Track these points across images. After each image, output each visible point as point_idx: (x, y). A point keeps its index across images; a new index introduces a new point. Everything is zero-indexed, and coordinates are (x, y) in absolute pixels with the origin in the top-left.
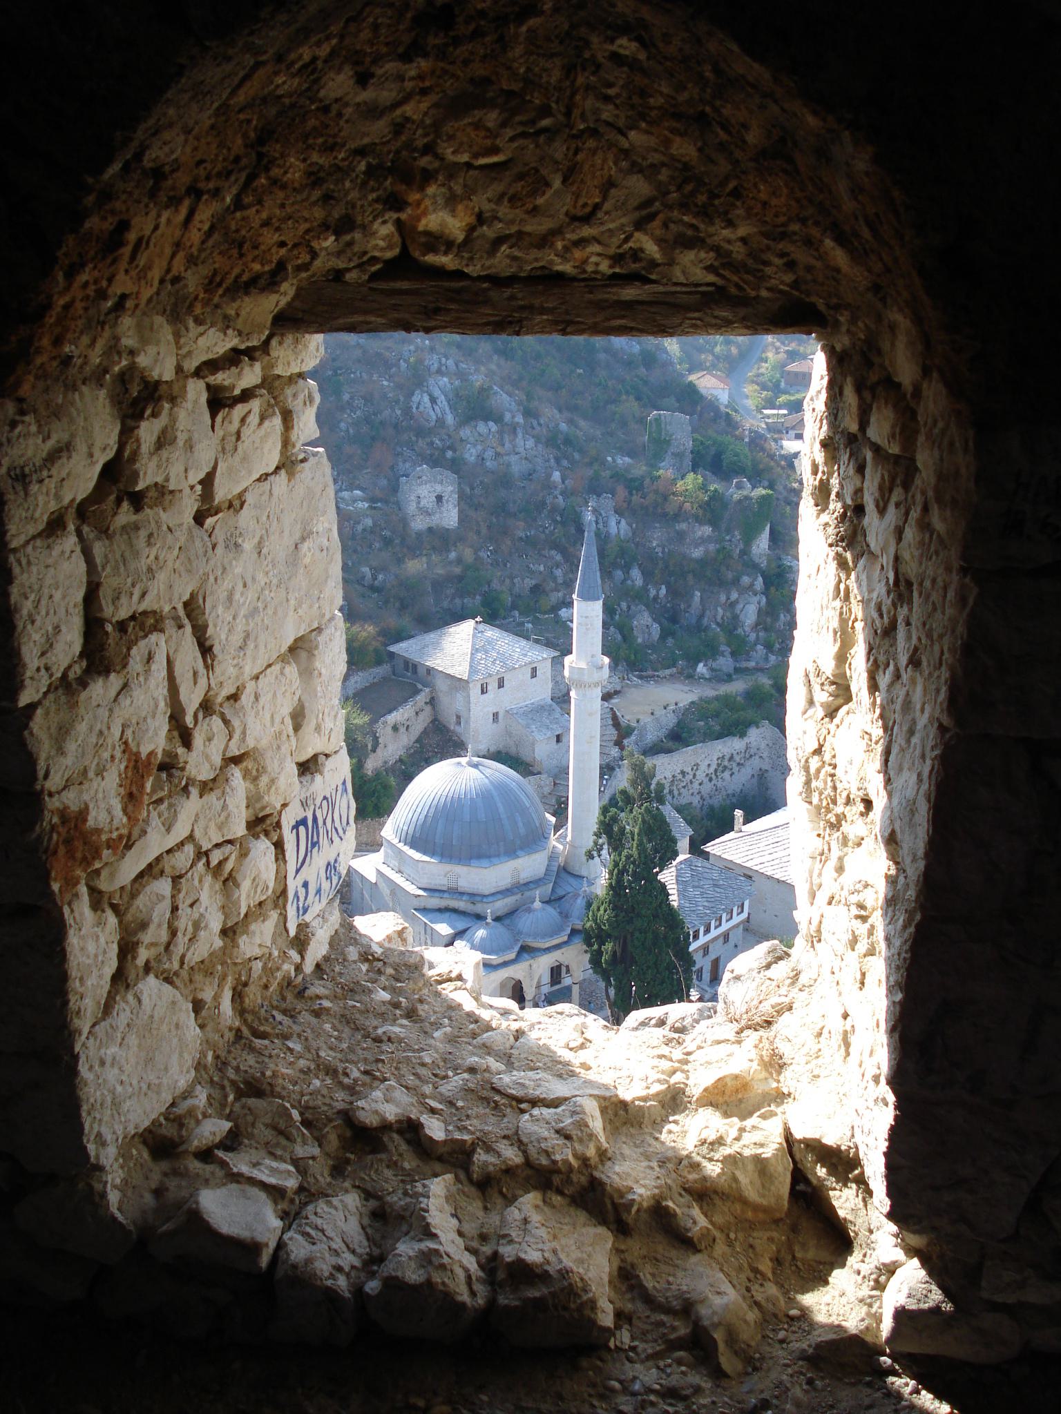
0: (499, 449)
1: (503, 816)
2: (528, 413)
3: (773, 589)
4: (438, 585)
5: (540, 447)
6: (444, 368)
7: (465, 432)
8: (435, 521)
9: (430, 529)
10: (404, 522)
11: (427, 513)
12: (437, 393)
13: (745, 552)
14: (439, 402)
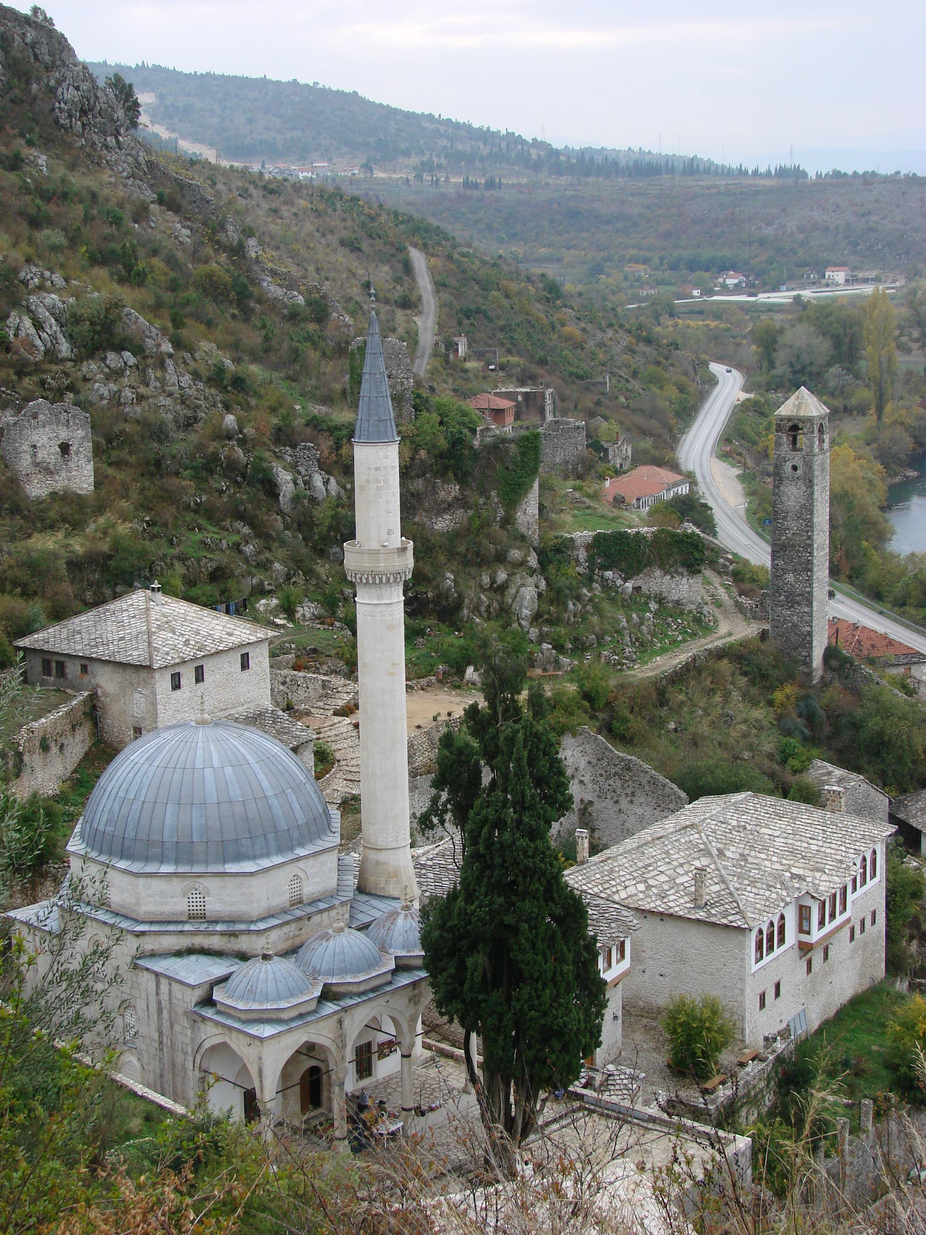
0: (142, 390)
1: (270, 793)
2: (178, 344)
3: (551, 569)
4: (75, 565)
5: (201, 385)
6: (49, 283)
7: (91, 367)
8: (59, 483)
9: (53, 495)
10: (14, 482)
11: (48, 471)
12: (43, 313)
13: (508, 521)
14: (47, 327)
